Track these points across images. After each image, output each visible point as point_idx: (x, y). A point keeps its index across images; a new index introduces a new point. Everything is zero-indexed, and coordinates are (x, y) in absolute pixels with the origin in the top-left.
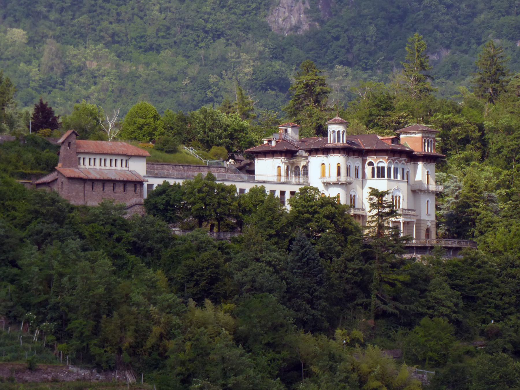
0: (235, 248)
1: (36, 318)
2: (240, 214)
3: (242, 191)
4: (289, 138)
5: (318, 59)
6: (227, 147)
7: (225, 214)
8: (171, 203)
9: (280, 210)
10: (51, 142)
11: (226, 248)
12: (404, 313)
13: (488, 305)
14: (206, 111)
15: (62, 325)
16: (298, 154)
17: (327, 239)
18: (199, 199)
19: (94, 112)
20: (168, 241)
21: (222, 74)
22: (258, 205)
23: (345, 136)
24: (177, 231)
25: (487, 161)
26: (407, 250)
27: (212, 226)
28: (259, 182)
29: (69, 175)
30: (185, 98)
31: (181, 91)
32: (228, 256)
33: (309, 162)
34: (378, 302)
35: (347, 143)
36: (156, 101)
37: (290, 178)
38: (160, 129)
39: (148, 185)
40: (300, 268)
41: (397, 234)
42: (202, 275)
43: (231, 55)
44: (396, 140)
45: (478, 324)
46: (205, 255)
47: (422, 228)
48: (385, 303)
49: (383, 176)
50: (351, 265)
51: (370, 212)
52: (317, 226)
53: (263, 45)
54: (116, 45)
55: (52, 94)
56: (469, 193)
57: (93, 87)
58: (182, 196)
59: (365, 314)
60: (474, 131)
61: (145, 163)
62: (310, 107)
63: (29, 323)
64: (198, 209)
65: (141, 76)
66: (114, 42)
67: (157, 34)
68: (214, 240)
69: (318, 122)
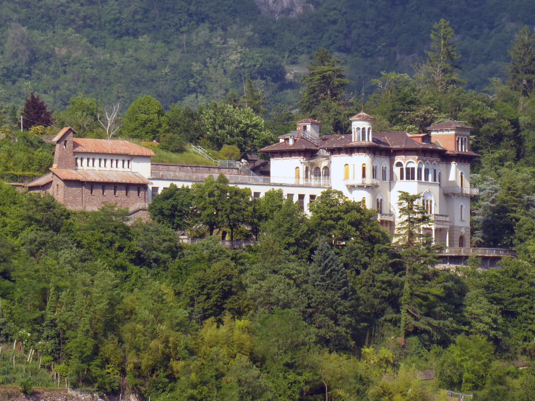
0: (250, 258)
1: (31, 336)
2: (256, 220)
3: (257, 194)
4: (308, 136)
5: (313, 45)
6: (240, 146)
7: (239, 221)
8: (178, 208)
9: (300, 216)
10: (44, 140)
11: (240, 258)
12: (438, 329)
13: (530, 321)
14: (216, 106)
15: (59, 344)
16: (318, 154)
17: (352, 249)
18: (210, 204)
19: (91, 107)
20: (175, 251)
21: (206, 61)
22: (275, 210)
23: (371, 133)
24: (185, 239)
25: (522, 161)
26: (441, 260)
27: (224, 234)
28: (276, 185)
29: (65, 178)
30: (164, 88)
31: (160, 81)
32: (243, 268)
33: (331, 162)
34: (409, 317)
35: (373, 141)
36: (133, 91)
37: (309, 180)
38: (165, 126)
39: (153, 188)
40: (323, 280)
41: (429, 242)
42: (213, 289)
43: (217, 40)
44: (427, 138)
45: (519, 342)
46: (217, 266)
47: (455, 236)
48: (416, 319)
49: (413, 178)
50: (379, 277)
51: (400, 219)
52: (342, 234)
53: (252, 30)
54: (88, 30)
55: (18, 84)
56: (506, 196)
57: (63, 76)
58: (191, 200)
59: (394, 331)
60: (506, 128)
61: (150, 164)
62: (327, 101)
63: (22, 342)
64: (208, 215)
65: (116, 63)
66: (85, 26)
67: (133, 17)
68: (227, 249)
69: (337, 117)
